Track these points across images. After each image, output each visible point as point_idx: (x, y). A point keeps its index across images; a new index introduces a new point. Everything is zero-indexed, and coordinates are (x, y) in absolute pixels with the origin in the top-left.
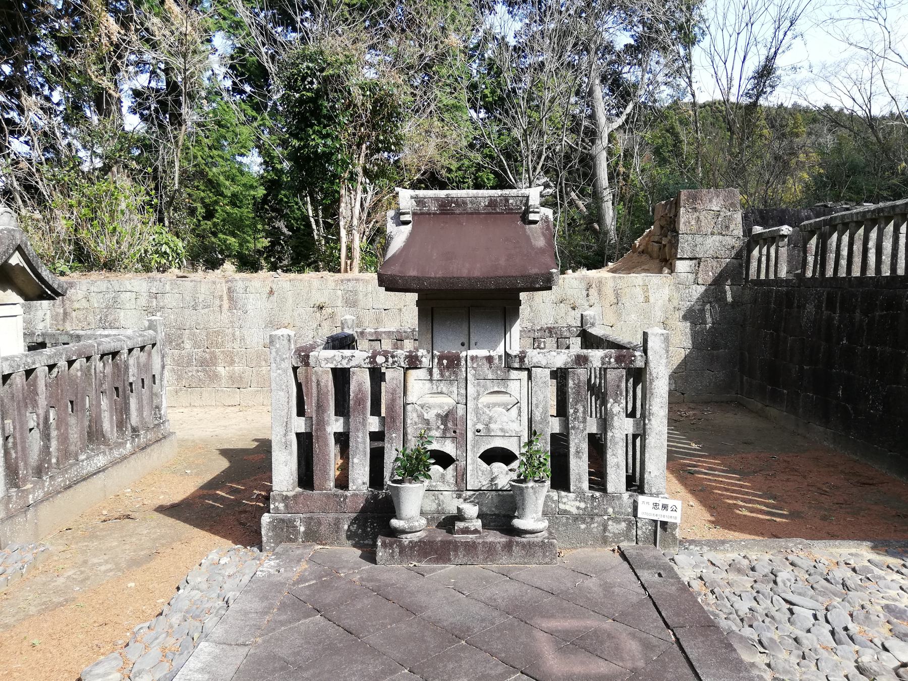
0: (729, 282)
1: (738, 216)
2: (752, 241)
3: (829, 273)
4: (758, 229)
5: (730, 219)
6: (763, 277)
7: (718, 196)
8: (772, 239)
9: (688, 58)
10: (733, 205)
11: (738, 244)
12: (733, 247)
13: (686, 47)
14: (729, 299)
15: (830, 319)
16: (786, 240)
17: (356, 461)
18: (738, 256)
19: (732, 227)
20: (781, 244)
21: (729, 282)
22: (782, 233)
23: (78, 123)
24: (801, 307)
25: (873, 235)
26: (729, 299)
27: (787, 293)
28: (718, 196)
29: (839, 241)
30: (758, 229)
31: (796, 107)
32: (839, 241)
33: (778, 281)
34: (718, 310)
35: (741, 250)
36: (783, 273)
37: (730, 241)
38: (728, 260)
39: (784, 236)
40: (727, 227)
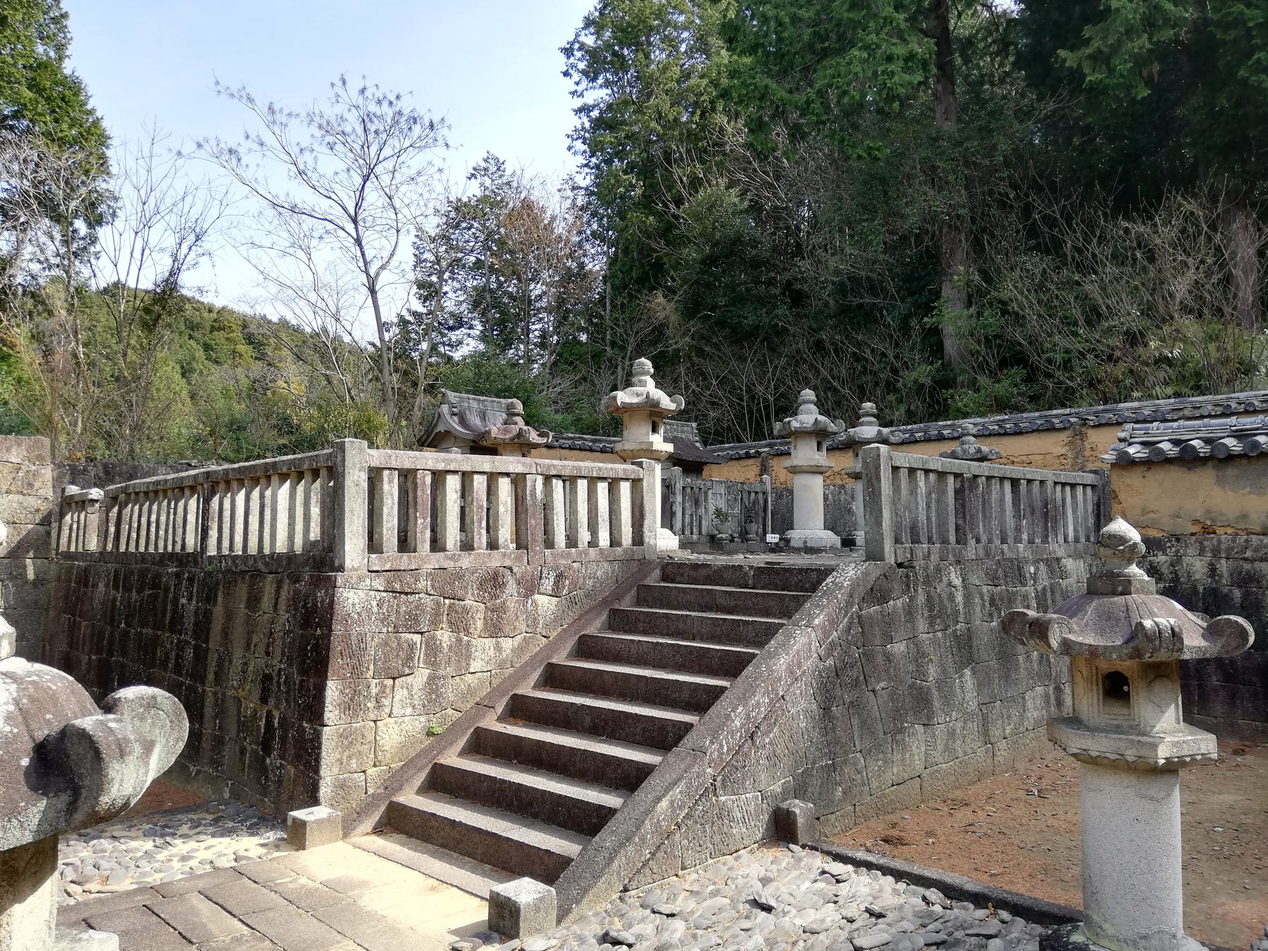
0: (31, 554)
1: (48, 473)
2: (68, 504)
3: (122, 549)
4: (73, 490)
5: (36, 475)
6: (73, 549)
7: (19, 445)
8: (82, 504)
9: (94, 240)
10: (40, 458)
11: (45, 507)
12: (38, 510)
13: (90, 225)
14: (31, 575)
15: (115, 599)
16: (97, 505)
17: (25, 762)
18: (46, 521)
19: (37, 485)
20: (90, 510)
21: (31, 554)
22: (90, 497)
23: (715, 83)
24: (95, 586)
25: (155, 507)
26: (31, 575)
27: (86, 569)
28: (19, 445)
29: (132, 510)
30: (73, 490)
31: (284, 323)
32: (132, 510)
33: (86, 555)
34: (13, 590)
35: (50, 514)
36: (93, 545)
37: (32, 502)
38: (30, 526)
39: (93, 501)
40: (30, 485)
